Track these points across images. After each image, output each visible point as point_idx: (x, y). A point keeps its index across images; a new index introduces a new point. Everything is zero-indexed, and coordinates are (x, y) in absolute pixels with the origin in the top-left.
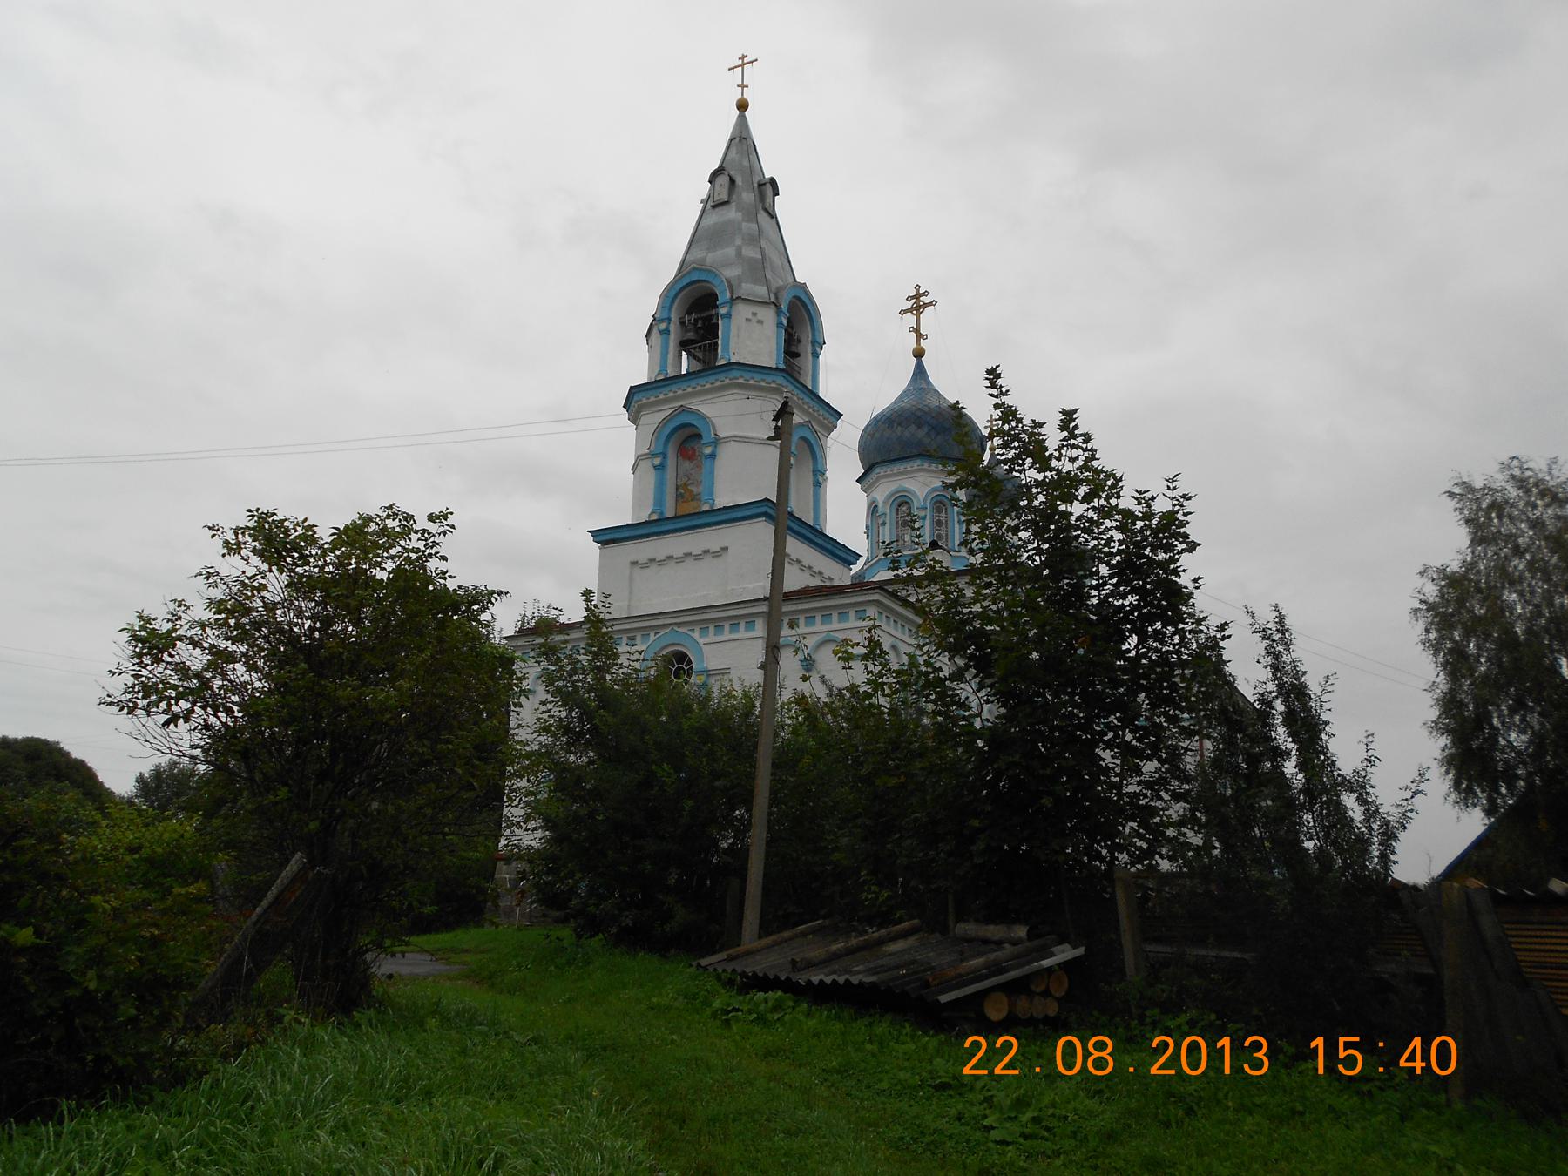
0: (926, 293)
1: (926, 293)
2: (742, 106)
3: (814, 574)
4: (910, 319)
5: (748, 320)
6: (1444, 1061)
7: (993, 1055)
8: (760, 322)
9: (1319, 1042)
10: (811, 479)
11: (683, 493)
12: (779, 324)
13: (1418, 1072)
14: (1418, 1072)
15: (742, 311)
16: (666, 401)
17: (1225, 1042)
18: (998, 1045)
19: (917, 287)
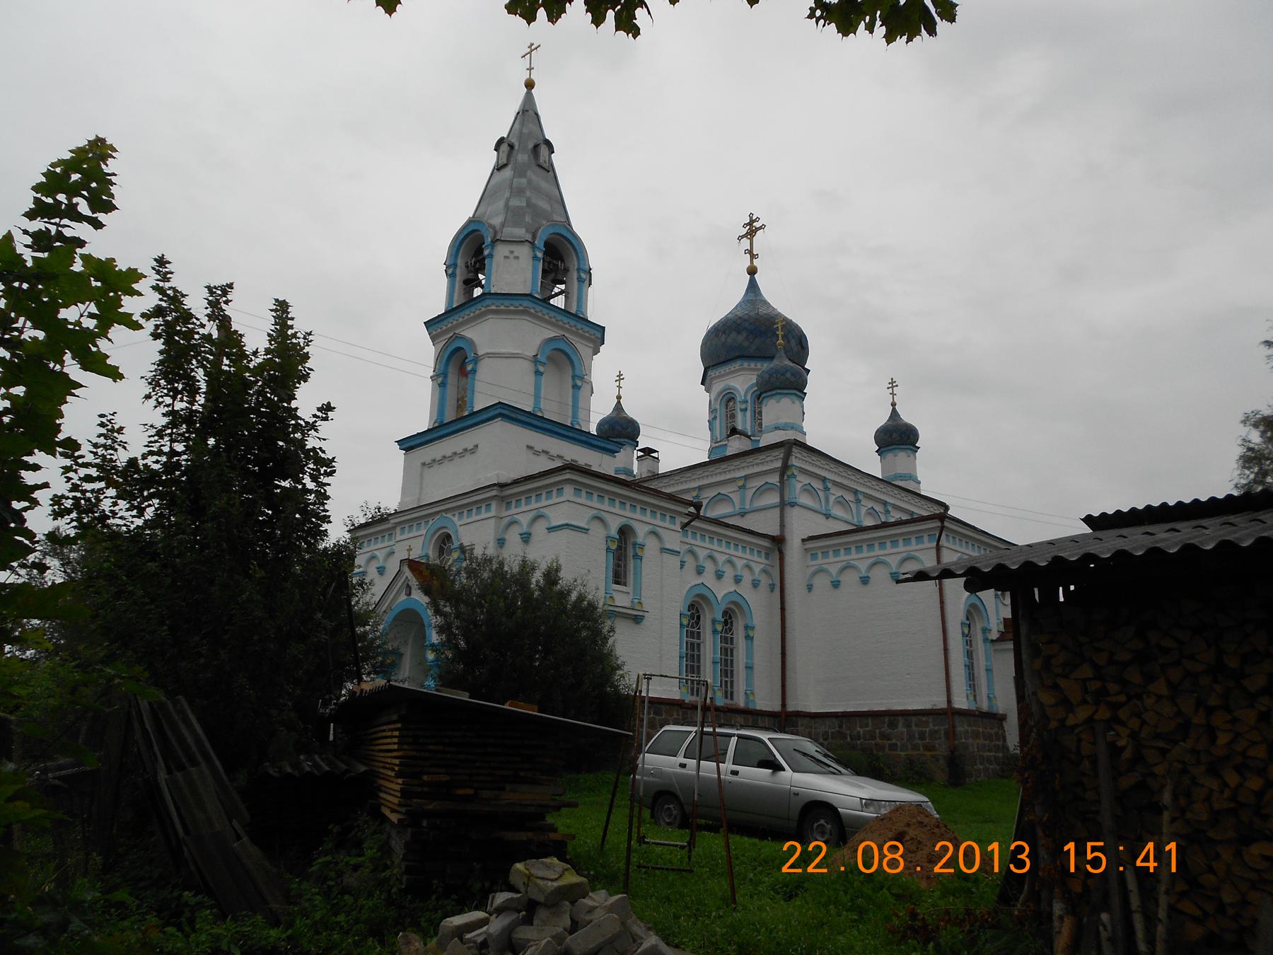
0: (757, 219)
1: (757, 219)
2: (530, 85)
3: (552, 458)
4: (746, 243)
5: (506, 257)
6: (868, 852)
7: (805, 859)
8: (517, 258)
9: (1071, 846)
10: (570, 383)
11: (461, 403)
12: (535, 258)
13: (1152, 870)
14: (1152, 870)
15: (501, 251)
16: (562, 328)
17: (995, 846)
18: (810, 849)
19: (751, 215)
